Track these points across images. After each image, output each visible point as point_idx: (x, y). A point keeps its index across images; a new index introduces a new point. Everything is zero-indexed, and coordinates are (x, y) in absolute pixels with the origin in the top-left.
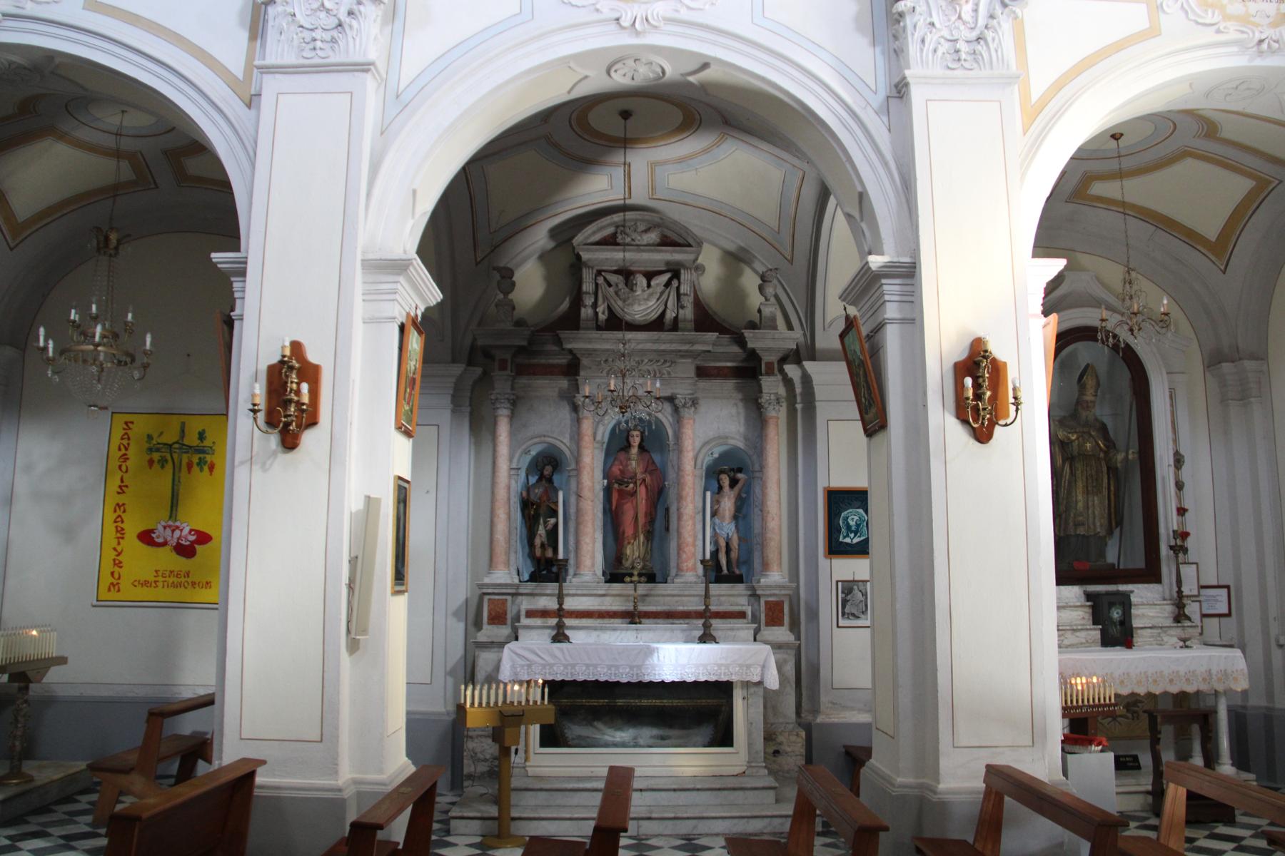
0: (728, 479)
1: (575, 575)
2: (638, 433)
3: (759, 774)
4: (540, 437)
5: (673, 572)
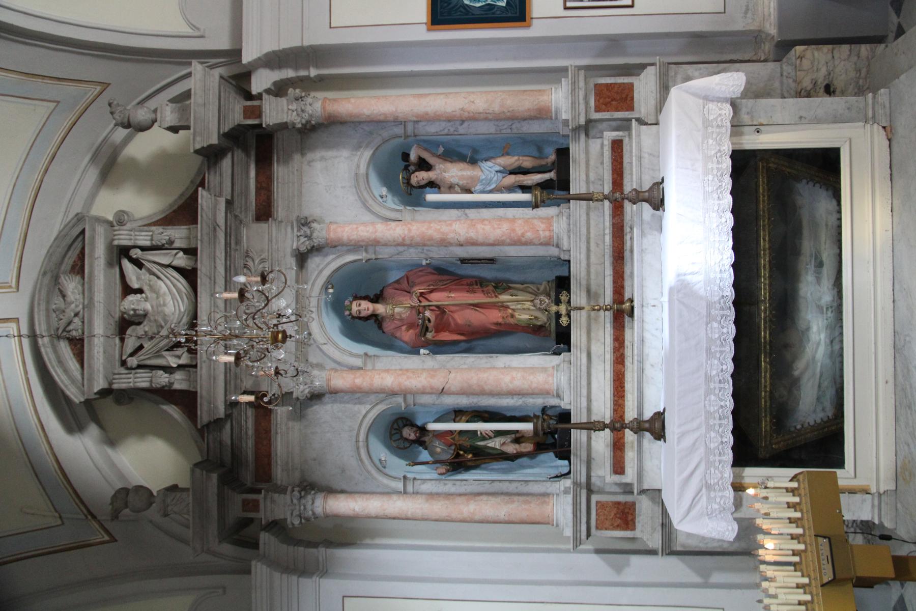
0: (417, 173)
1: (558, 396)
2: (354, 303)
3: (887, 105)
4: (358, 448)
5: (553, 251)
